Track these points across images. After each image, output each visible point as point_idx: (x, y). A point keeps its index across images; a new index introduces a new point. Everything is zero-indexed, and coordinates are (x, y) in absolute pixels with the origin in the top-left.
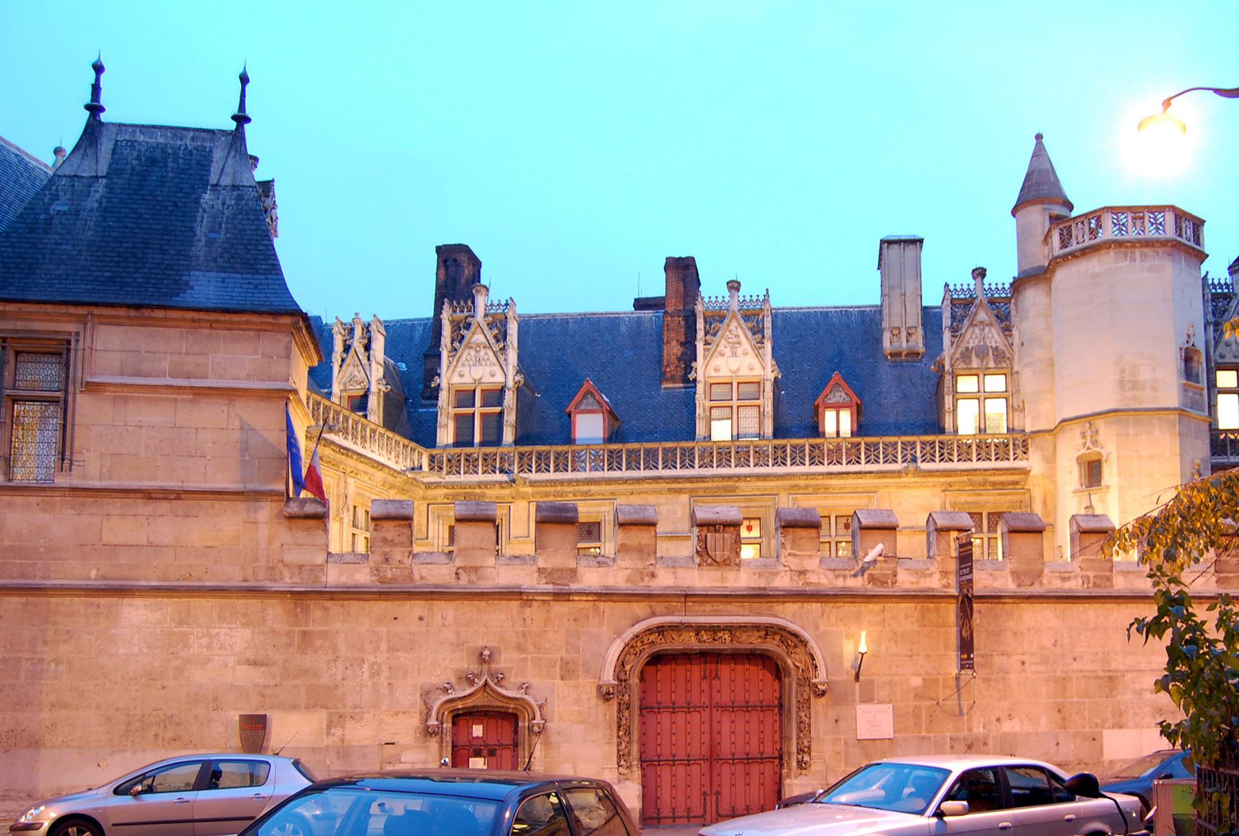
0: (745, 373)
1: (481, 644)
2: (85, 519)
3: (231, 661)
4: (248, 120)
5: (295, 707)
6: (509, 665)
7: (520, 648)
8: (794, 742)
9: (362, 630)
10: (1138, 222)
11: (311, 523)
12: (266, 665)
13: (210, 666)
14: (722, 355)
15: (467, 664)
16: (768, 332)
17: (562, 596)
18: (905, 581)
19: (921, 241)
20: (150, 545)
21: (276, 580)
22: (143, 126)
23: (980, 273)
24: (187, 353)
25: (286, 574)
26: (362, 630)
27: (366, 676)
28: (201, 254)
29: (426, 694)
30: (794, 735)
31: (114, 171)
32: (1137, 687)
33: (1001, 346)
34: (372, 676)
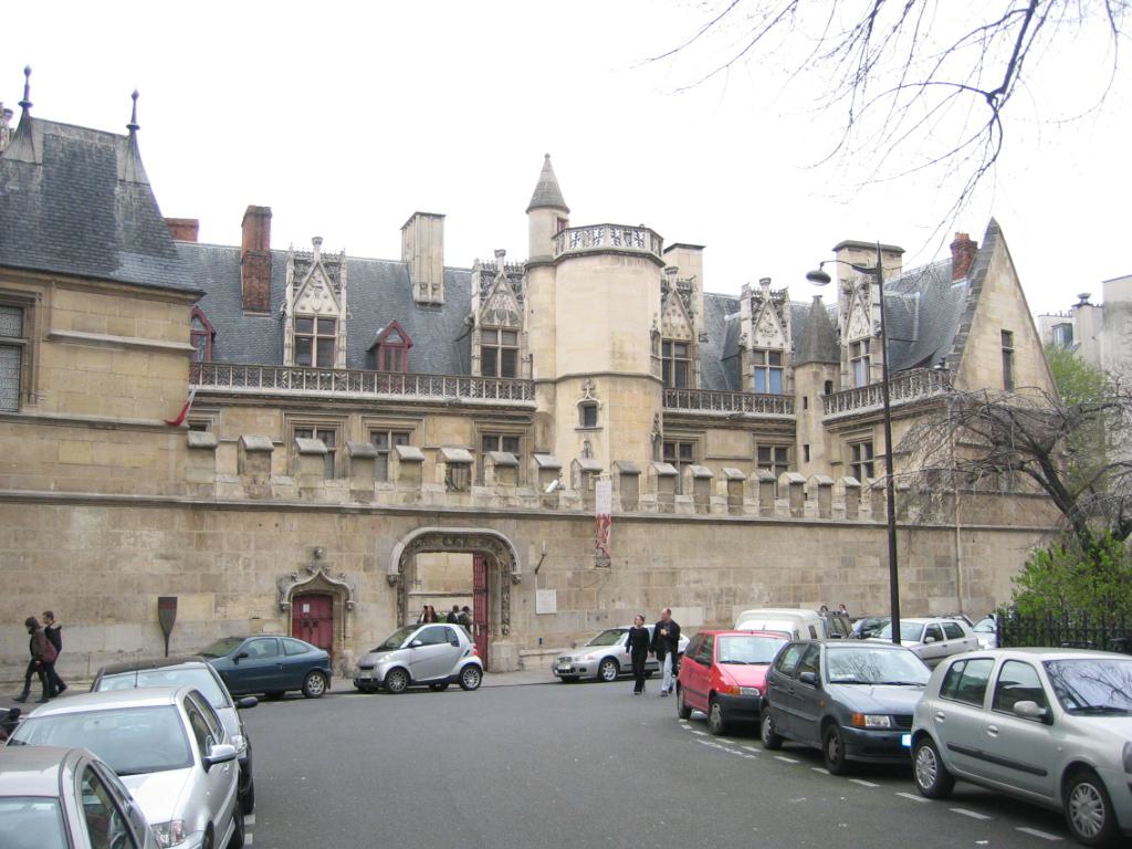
0: (324, 312)
1: (314, 545)
2: (46, 442)
3: (150, 556)
4: (137, 128)
5: (193, 591)
6: (331, 561)
7: (339, 548)
8: (500, 615)
10: (628, 237)
11: (206, 452)
12: (174, 559)
13: (136, 559)
14: (308, 296)
15: (305, 560)
17: (366, 512)
18: (564, 507)
19: (444, 216)
22: (62, 124)
23: (501, 253)
24: (120, 316)
25: (188, 490)
27: (241, 567)
28: (122, 236)
29: (279, 581)
30: (500, 610)
31: (47, 161)
32: (687, 579)
33: (515, 310)
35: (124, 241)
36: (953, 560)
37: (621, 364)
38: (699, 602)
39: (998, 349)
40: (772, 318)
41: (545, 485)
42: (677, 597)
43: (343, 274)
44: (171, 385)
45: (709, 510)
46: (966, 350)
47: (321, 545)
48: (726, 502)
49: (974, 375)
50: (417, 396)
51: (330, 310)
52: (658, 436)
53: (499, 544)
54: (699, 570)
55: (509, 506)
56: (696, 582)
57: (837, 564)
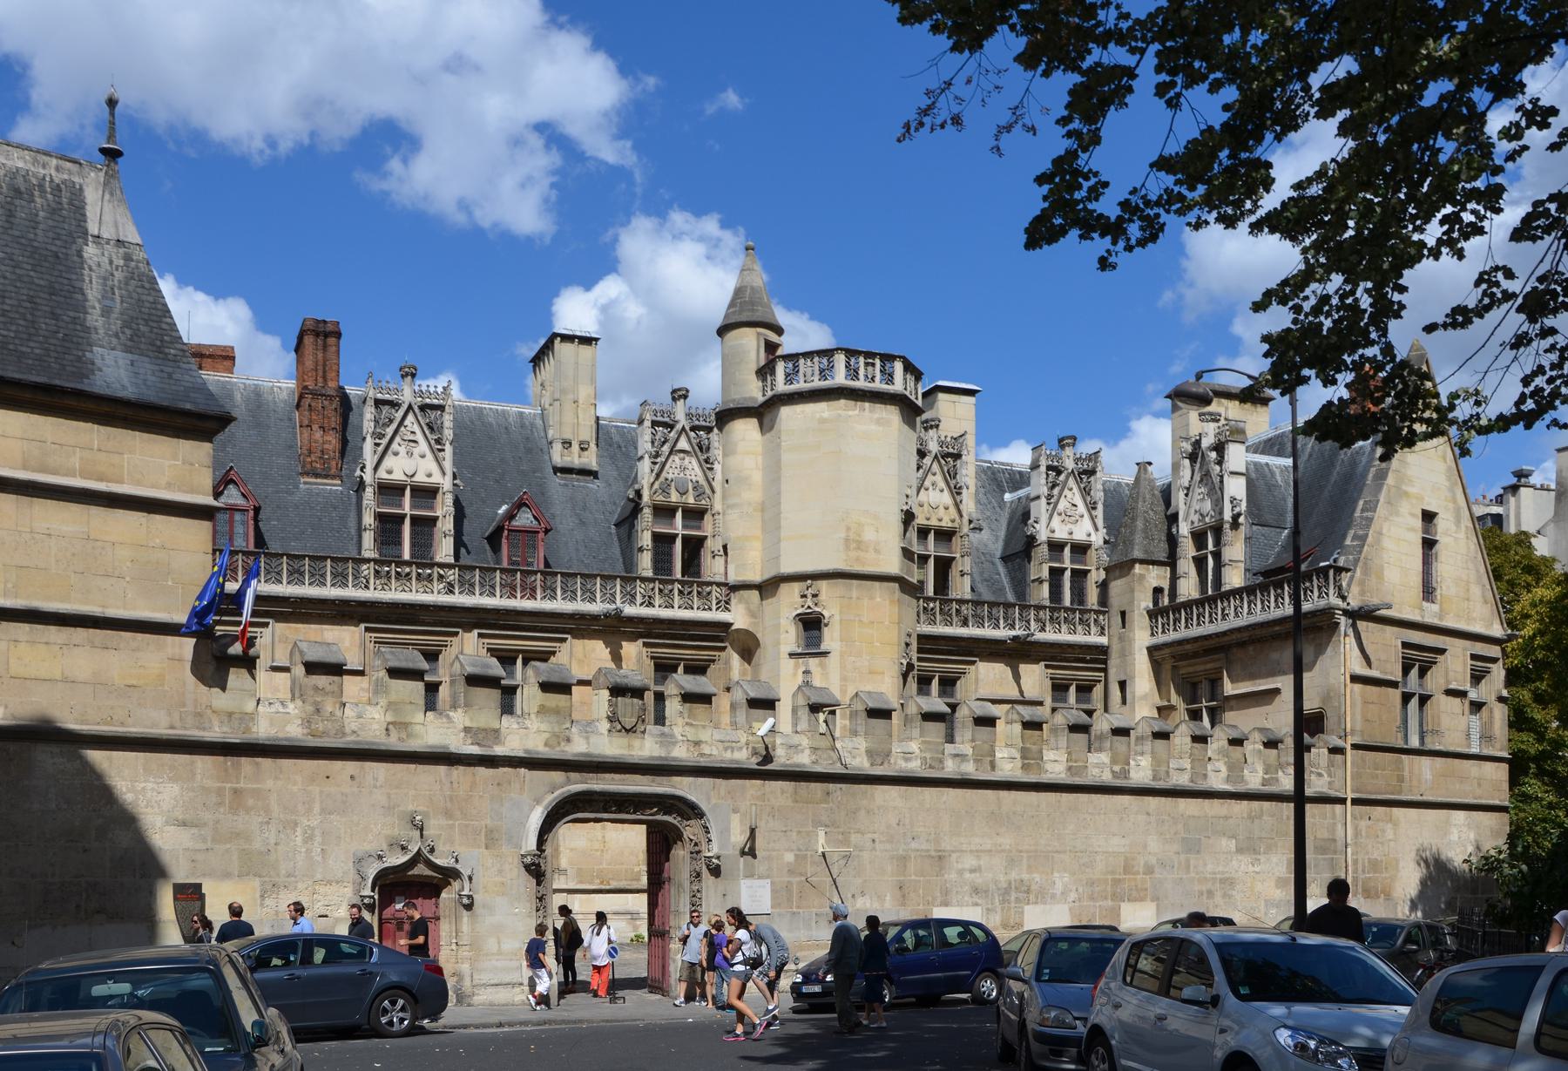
0: (420, 478)
1: (411, 808)
5: (227, 875)
7: (448, 814)
9: (295, 789)
14: (396, 454)
16: (448, 434)
20: (65, 680)
21: (204, 729)
25: (216, 723)
26: (295, 789)
27: (299, 840)
34: (305, 841)
35: (101, 331)
36: (1340, 844)
37: (858, 559)
38: (976, 899)
39: (1416, 539)
40: (1073, 495)
41: (755, 725)
42: (946, 892)
43: (448, 420)
44: (178, 564)
45: (993, 766)
46: (1370, 539)
47: (420, 808)
48: (1018, 756)
49: (1380, 576)
50: (559, 605)
51: (429, 475)
52: (910, 667)
53: (690, 810)
54: (977, 853)
55: (702, 755)
56: (972, 871)
57: (1176, 847)
